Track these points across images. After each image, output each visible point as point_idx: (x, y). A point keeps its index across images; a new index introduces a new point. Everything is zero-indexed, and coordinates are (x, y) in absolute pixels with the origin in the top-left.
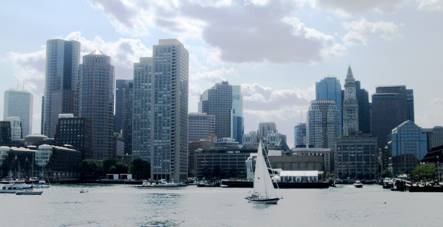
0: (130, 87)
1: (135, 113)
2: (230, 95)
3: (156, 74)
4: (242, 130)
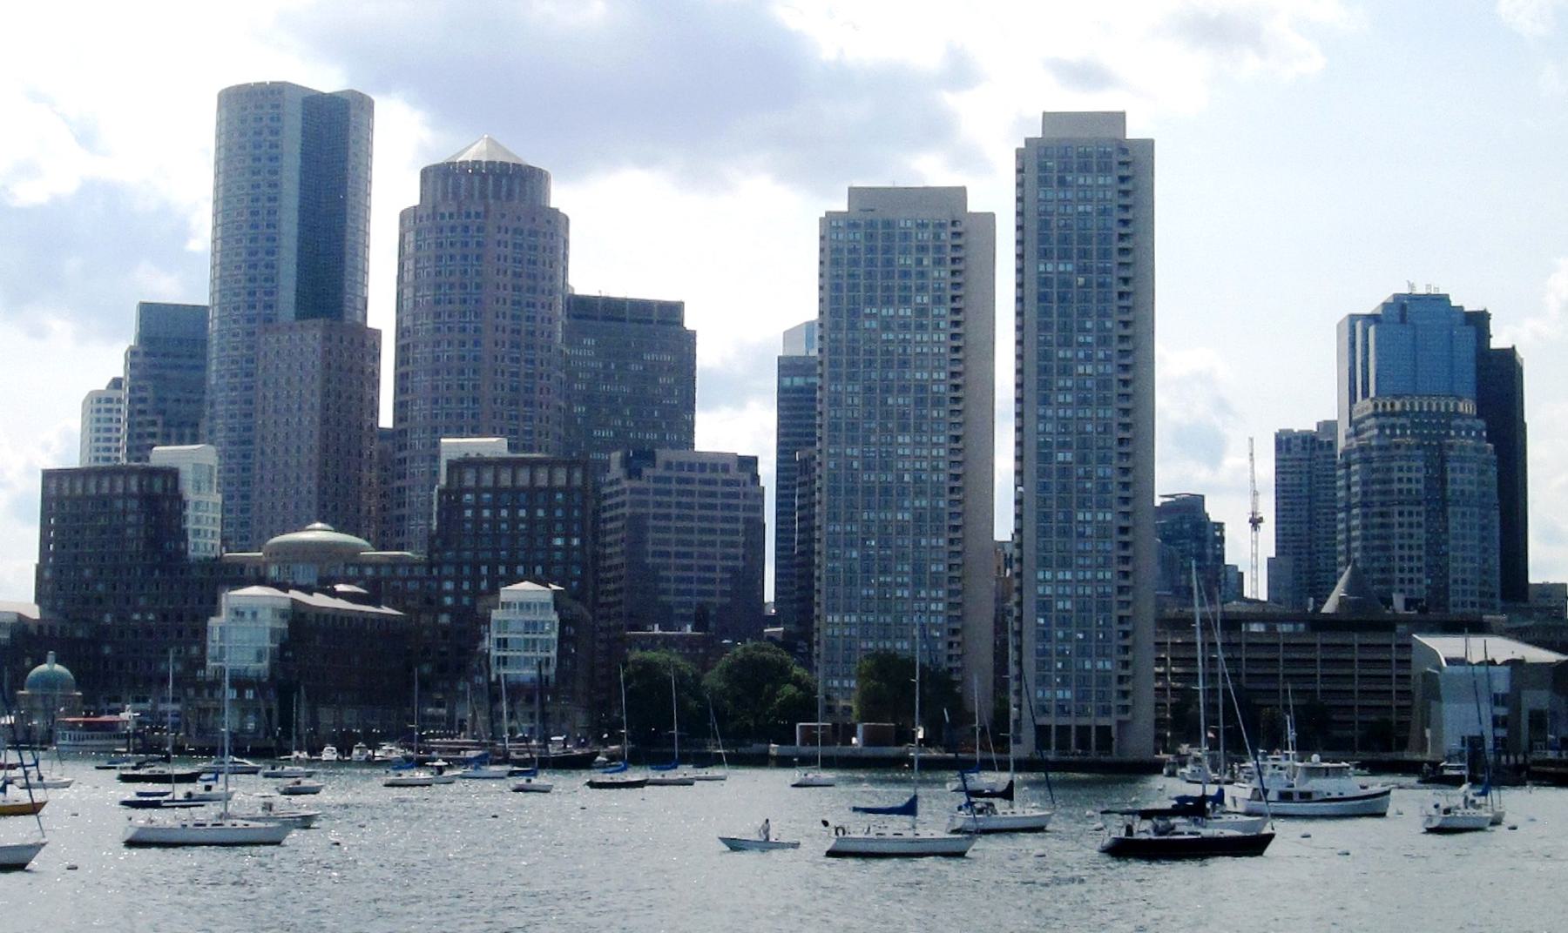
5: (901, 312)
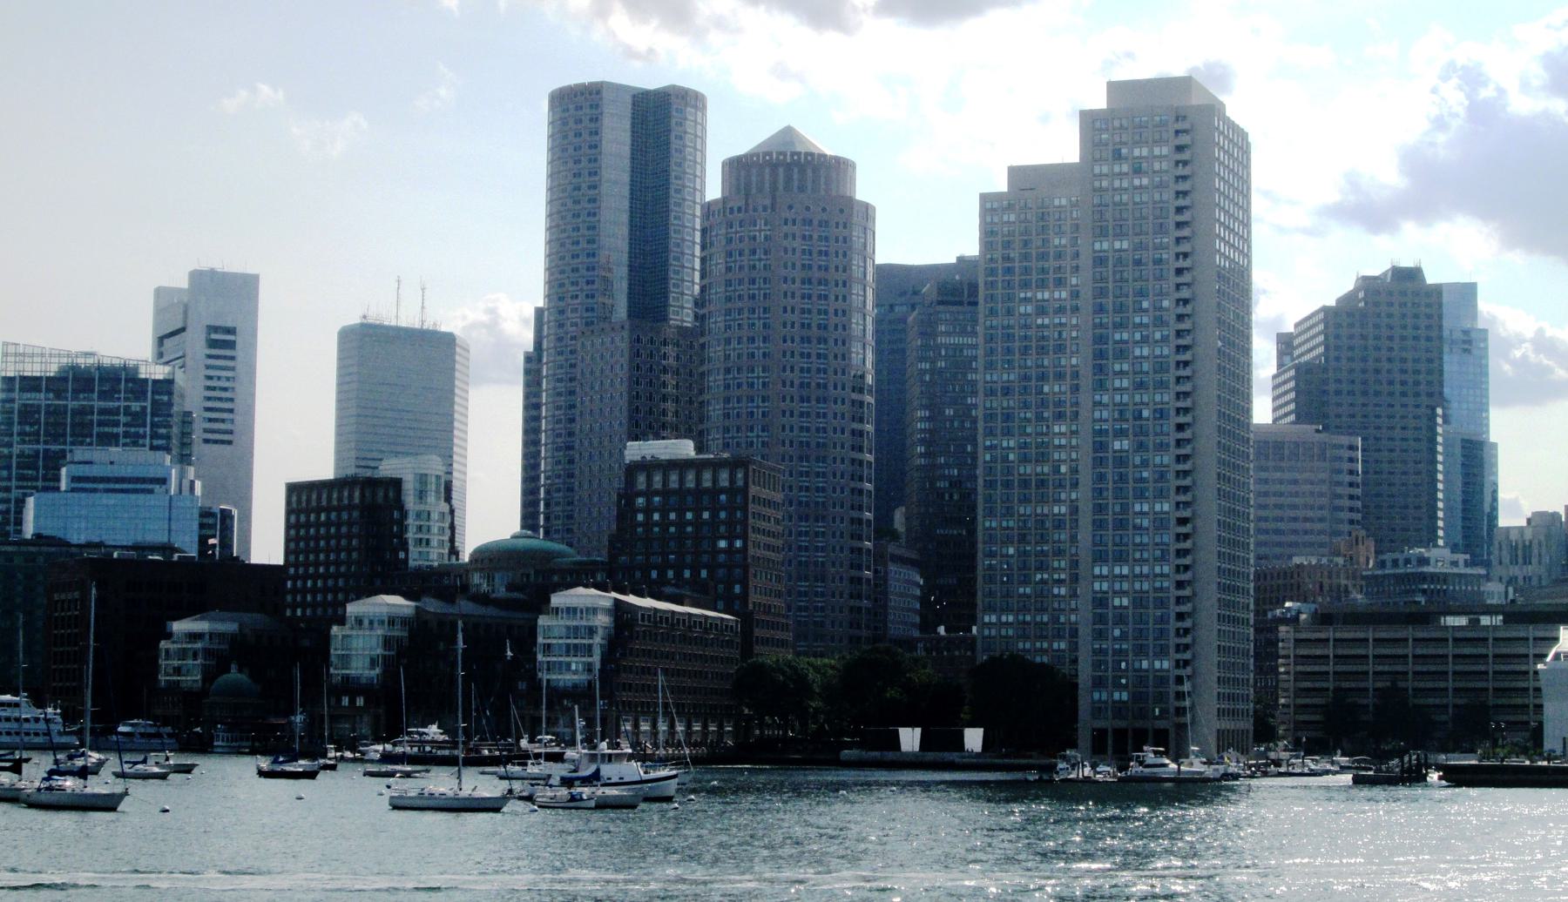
0: (940, 303)
1: (990, 433)
2: (1434, 334)
3: (1097, 246)
4: (1487, 509)
5: (1057, 295)
